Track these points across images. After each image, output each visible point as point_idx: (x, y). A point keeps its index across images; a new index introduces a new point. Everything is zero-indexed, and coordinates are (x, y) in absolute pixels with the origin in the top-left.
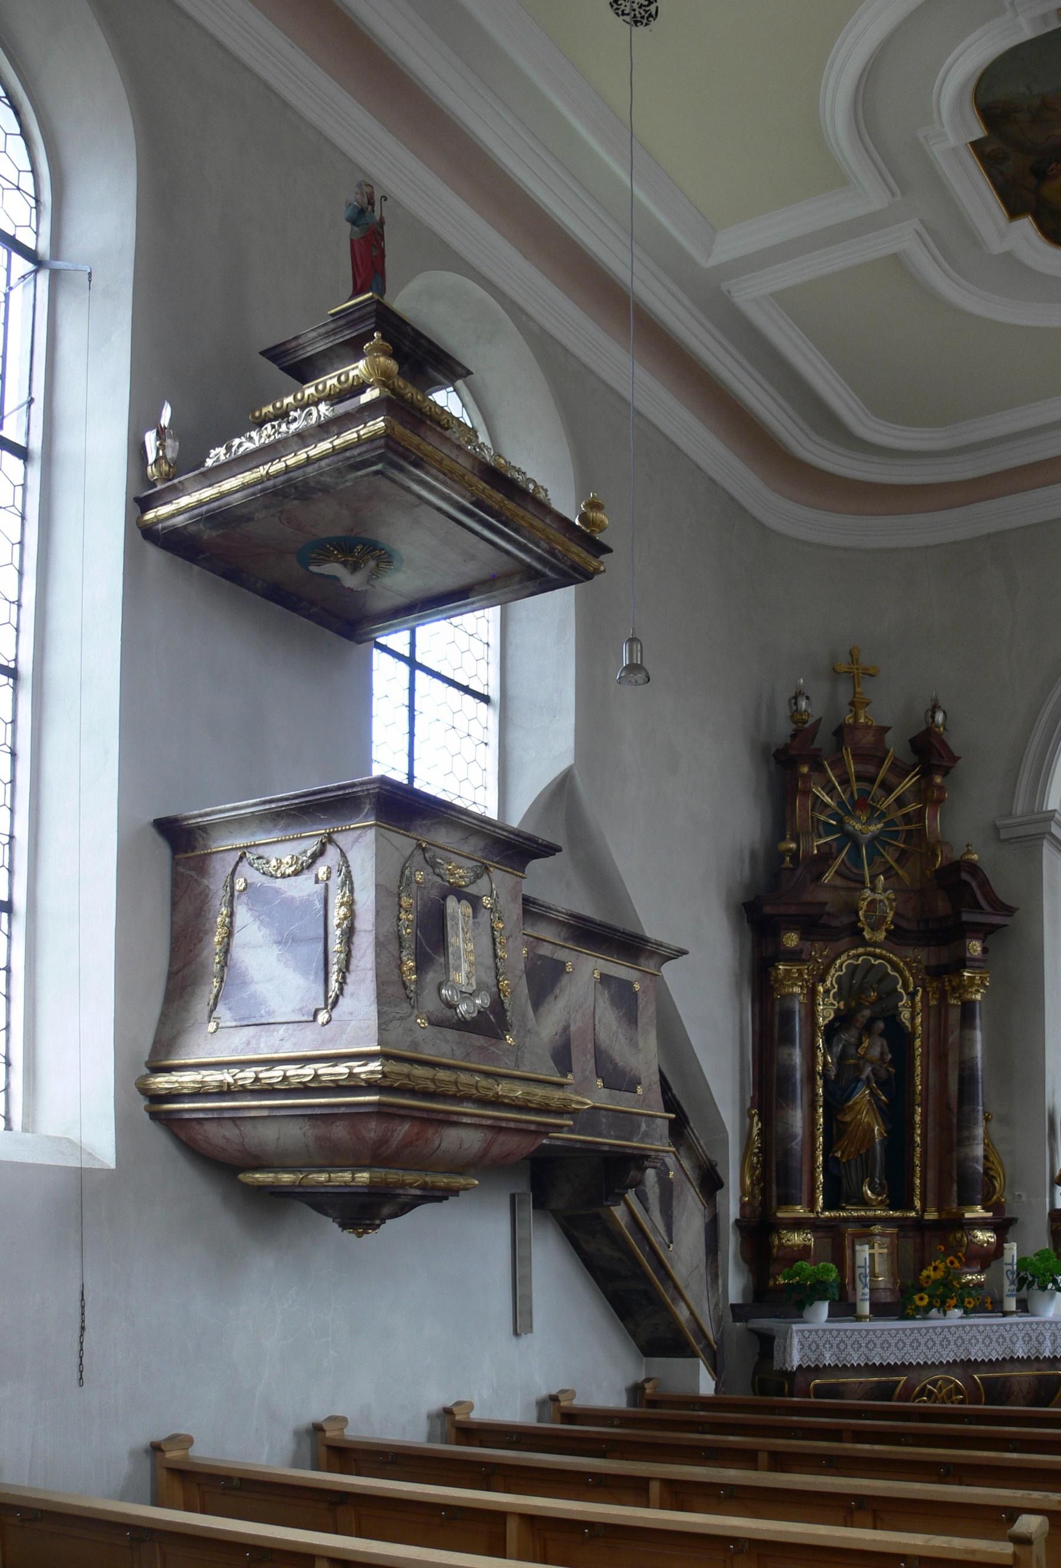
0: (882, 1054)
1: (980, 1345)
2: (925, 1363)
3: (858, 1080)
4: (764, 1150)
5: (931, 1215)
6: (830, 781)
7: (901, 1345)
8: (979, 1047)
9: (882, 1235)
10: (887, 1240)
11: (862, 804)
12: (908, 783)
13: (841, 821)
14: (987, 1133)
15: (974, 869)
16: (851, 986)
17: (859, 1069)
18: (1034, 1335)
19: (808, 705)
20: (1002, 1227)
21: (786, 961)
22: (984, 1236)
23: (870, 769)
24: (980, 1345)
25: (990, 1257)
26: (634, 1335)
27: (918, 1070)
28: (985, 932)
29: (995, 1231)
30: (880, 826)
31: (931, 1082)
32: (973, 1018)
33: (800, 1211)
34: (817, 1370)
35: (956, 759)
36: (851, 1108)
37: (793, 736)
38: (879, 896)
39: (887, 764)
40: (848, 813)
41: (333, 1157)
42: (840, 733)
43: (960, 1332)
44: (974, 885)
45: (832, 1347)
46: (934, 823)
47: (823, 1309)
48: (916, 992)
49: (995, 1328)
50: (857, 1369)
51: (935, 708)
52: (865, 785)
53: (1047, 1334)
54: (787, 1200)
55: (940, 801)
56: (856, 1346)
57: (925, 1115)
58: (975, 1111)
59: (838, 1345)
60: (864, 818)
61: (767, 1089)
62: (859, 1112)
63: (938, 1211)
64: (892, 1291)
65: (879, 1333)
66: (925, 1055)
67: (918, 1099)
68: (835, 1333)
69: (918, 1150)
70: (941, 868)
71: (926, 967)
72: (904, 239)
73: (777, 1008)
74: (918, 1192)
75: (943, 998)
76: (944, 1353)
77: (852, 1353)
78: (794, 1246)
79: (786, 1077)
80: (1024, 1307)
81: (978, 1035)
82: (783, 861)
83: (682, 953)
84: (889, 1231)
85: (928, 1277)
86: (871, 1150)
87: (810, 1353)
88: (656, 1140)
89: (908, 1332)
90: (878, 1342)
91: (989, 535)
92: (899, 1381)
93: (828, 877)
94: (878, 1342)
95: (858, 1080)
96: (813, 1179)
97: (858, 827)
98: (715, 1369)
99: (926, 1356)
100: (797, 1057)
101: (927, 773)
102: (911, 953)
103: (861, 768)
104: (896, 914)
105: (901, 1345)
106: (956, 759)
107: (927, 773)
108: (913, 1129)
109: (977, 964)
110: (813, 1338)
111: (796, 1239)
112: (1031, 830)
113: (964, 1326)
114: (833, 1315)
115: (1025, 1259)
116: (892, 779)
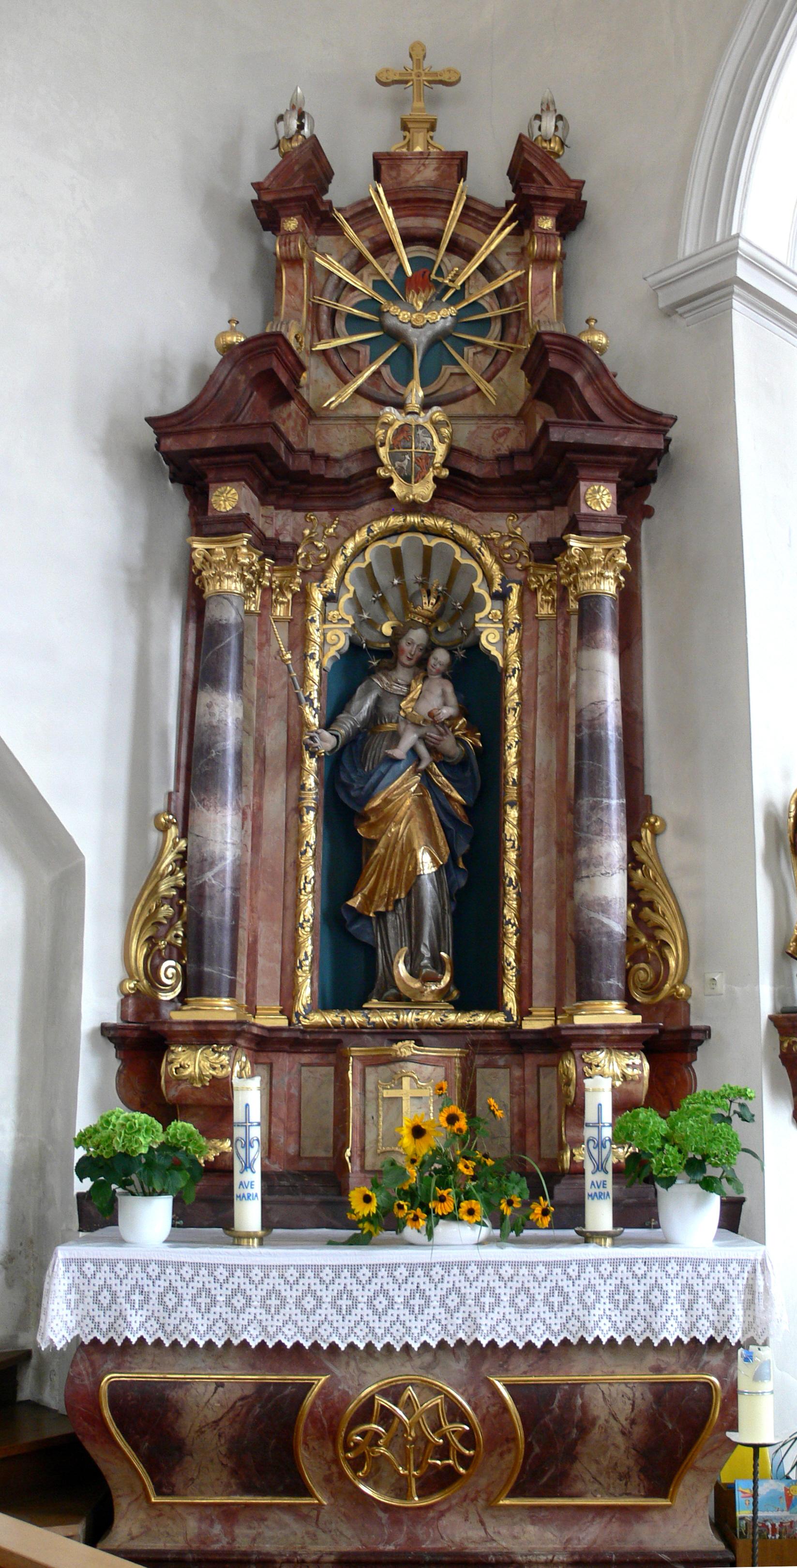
2: (370, 1345)
7: (309, 1302)
13: (380, 313)
18: (639, 1290)
27: (513, 736)
33: (221, 1009)
39: (456, 210)
40: (393, 298)
43: (455, 1277)
45: (147, 1300)
49: (540, 1271)
52: (422, 251)
53: (672, 1289)
54: (194, 986)
56: (203, 1300)
59: (161, 1296)
65: (327, 1274)
67: (512, 793)
68: (573, 1270)
71: (532, 546)
74: (511, 974)
76: (416, 1326)
77: (195, 1315)
89: (327, 1274)
90: (256, 1295)
92: (310, 1385)
94: (256, 1295)
99: (372, 1330)
102: (501, 524)
109: (600, 527)
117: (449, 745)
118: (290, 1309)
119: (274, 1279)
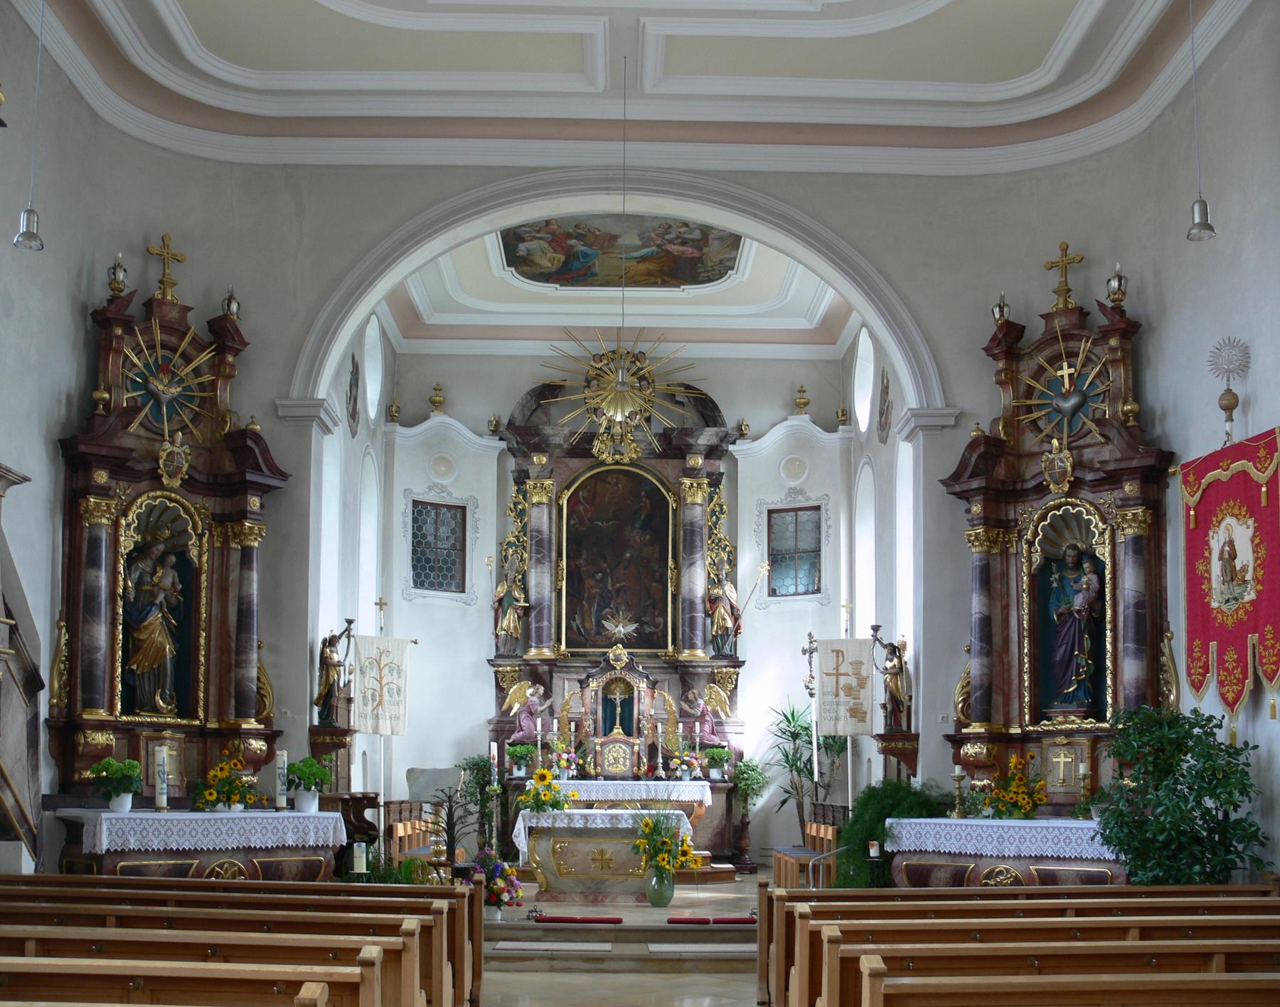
0: (173, 584)
1: (259, 834)
3: (153, 604)
4: (71, 658)
5: (212, 725)
6: (139, 345)
8: (255, 586)
9: (172, 739)
10: (176, 744)
11: (164, 368)
12: (204, 357)
13: (146, 380)
14: (259, 660)
15: (257, 437)
16: (148, 523)
17: (153, 595)
18: (301, 828)
19: (125, 276)
20: (271, 737)
21: (96, 495)
22: (258, 745)
23: (174, 340)
24: (259, 834)
25: (259, 763)
27: (204, 601)
28: (263, 490)
29: (266, 741)
30: (179, 389)
31: (214, 612)
32: (251, 561)
33: (102, 714)
34: (122, 854)
35: (245, 344)
36: (146, 628)
37: (110, 302)
38: (176, 451)
39: (188, 339)
40: (153, 374)
42: (149, 305)
44: (257, 451)
46: (224, 394)
48: (203, 534)
50: (157, 853)
51: (230, 299)
52: (168, 353)
53: (312, 827)
54: (90, 704)
55: (230, 377)
57: (208, 638)
58: (250, 639)
60: (165, 381)
61: (75, 604)
62: (152, 632)
63: (219, 721)
64: (180, 788)
65: (163, 822)
66: (210, 588)
67: (203, 625)
68: (138, 822)
69: (202, 668)
70: (230, 433)
71: (213, 514)
73: (86, 535)
74: (201, 704)
75: (226, 542)
76: (230, 841)
78: (96, 745)
79: (92, 597)
80: (292, 805)
81: (255, 576)
82: (96, 407)
83: (26, 479)
84: (178, 736)
85: (215, 776)
86: (162, 665)
87: (116, 838)
88: (842, 693)
89: (188, 822)
90: (175, 830)
91: (285, 165)
93: (133, 427)
94: (175, 830)
95: (153, 604)
96: (113, 687)
97: (161, 387)
98: (35, 851)
100: (103, 579)
101: (221, 351)
102: (200, 501)
103: (166, 338)
104: (190, 466)
105: (194, 833)
106: (245, 344)
107: (221, 351)
108: (198, 650)
110: (117, 826)
111: (100, 738)
112: (304, 412)
113: (245, 818)
115: (293, 765)
116: (192, 352)
117: (173, 601)
118: (187, 835)
119: (181, 824)
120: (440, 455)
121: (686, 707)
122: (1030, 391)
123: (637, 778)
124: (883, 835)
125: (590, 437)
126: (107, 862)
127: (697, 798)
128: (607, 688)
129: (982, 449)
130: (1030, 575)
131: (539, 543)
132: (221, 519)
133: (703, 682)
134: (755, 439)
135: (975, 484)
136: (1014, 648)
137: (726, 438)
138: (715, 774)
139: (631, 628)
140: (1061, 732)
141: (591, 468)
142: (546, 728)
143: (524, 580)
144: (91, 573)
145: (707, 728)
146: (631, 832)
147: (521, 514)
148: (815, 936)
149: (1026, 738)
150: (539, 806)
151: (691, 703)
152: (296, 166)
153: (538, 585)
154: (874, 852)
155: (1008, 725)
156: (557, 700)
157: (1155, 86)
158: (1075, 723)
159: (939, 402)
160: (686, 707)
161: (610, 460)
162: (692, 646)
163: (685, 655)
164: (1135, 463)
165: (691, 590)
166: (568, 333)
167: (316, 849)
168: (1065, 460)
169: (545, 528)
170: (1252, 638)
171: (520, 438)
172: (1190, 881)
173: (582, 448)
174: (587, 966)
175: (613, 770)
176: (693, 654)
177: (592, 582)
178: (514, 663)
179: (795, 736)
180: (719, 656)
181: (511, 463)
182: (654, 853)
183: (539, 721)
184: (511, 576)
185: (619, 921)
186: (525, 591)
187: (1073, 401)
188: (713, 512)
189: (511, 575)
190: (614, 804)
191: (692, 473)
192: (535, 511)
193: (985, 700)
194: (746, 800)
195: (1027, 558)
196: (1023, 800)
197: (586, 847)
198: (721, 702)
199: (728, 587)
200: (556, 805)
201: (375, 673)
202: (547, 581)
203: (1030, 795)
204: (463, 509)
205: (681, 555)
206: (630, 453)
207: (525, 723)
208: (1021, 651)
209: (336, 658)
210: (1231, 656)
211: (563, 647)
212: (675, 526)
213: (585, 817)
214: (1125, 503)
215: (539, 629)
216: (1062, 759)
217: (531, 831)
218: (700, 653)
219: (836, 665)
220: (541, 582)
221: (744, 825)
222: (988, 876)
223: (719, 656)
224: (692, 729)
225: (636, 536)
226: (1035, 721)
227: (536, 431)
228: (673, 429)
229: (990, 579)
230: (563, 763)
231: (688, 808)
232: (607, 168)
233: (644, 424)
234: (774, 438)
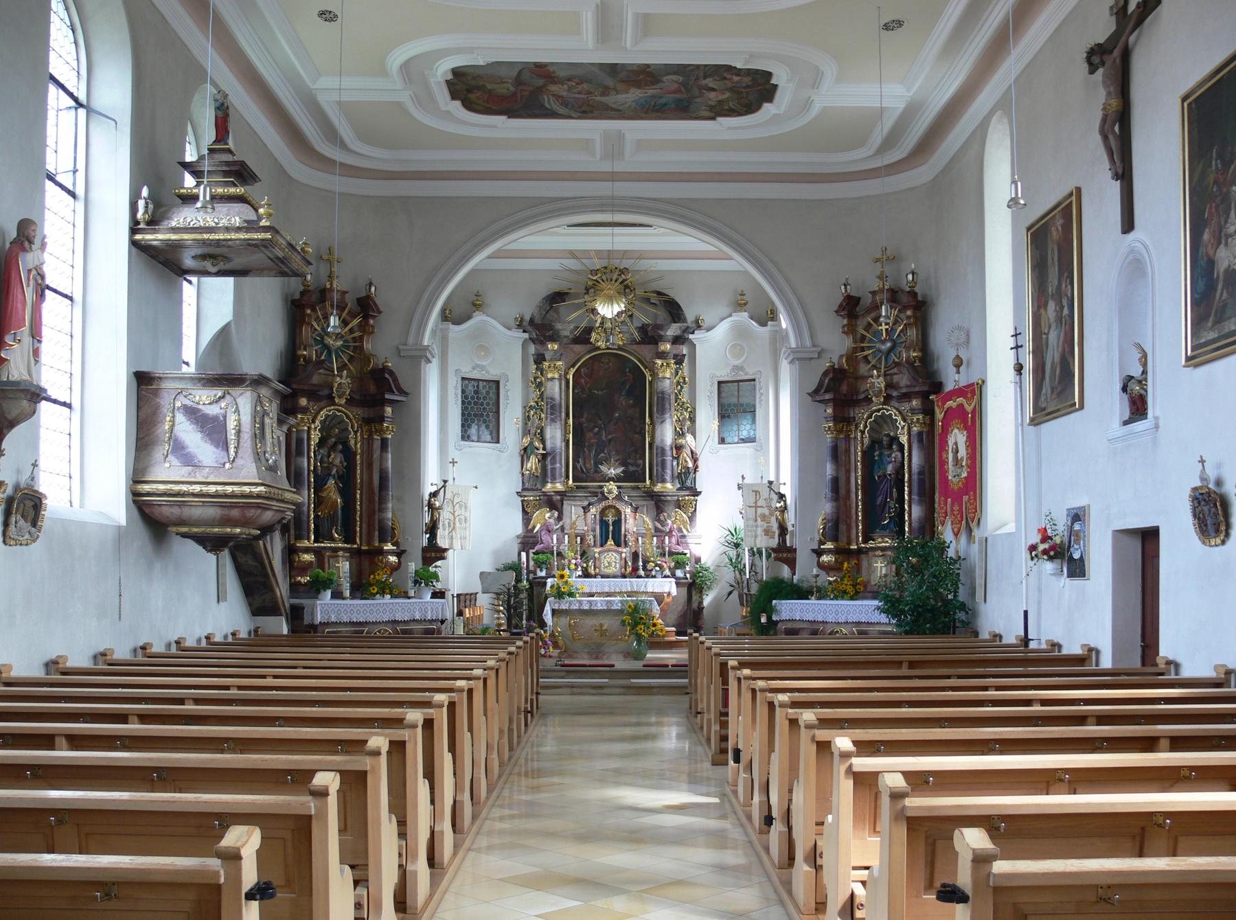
3: (330, 475)
12: (356, 322)
13: (322, 338)
15: (391, 373)
17: (329, 469)
20: (399, 554)
26: (250, 605)
33: (306, 543)
34: (327, 624)
35: (379, 312)
37: (303, 293)
38: (343, 381)
41: (226, 521)
46: (368, 346)
47: (329, 593)
50: (345, 624)
51: (371, 284)
66: (362, 464)
72: (405, 98)
86: (336, 512)
95: (330, 475)
101: (366, 317)
102: (355, 410)
110: (325, 608)
111: (308, 557)
114: (332, 597)
120: (481, 345)
121: (659, 526)
122: (863, 338)
123: (624, 576)
124: (770, 610)
125: (589, 330)
126: (320, 629)
127: (667, 590)
128: (603, 512)
129: (831, 375)
130: (862, 451)
131: (553, 407)
132: (368, 421)
133: (672, 507)
134: (708, 330)
135: (827, 397)
136: (853, 496)
137: (688, 330)
138: (679, 573)
139: (620, 470)
140: (879, 548)
141: (590, 352)
142: (560, 541)
143: (542, 434)
144: (299, 459)
145: (674, 540)
146: (621, 612)
147: (539, 385)
148: (794, 723)
149: (860, 551)
150: (560, 595)
151: (663, 523)
152: (408, 197)
153: (553, 437)
154: (763, 620)
155: (849, 543)
156: (566, 521)
157: (932, 161)
158: (888, 542)
159: (808, 343)
160: (659, 526)
161: (603, 346)
162: (664, 481)
163: (658, 487)
164: (917, 389)
165: (662, 440)
166: (573, 254)
167: (431, 621)
168: (880, 383)
169: (557, 396)
170: (965, 498)
171: (539, 330)
172: (924, 633)
173: (583, 338)
174: (594, 691)
175: (607, 571)
176: (662, 486)
177: (591, 435)
178: (537, 495)
179: (737, 545)
180: (683, 488)
181: (532, 349)
182: (635, 625)
183: (555, 537)
184: (533, 431)
185: (613, 666)
186: (543, 441)
187: (889, 345)
188: (678, 383)
189: (533, 430)
190: (609, 594)
191: (662, 355)
192: (549, 384)
193: (835, 528)
194: (701, 592)
195: (861, 439)
196: (850, 589)
197: (590, 622)
198: (684, 522)
199: (689, 437)
200: (571, 595)
201: (450, 509)
202: (559, 434)
203: (854, 586)
204: (497, 382)
205: (656, 415)
206: (618, 340)
207: (545, 537)
208: (857, 497)
209: (437, 504)
210: (956, 508)
211: (571, 482)
212: (651, 393)
213: (590, 602)
214: (913, 411)
215: (553, 470)
216: (879, 565)
217: (554, 612)
218: (669, 485)
219: (760, 498)
220: (555, 436)
221: (701, 609)
222: (831, 634)
223: (683, 488)
224: (663, 541)
225: (623, 401)
226: (865, 541)
227: (551, 328)
228: (648, 325)
229: (838, 454)
230: (573, 566)
231: (659, 598)
232: (600, 198)
233: (628, 320)
234: (722, 331)
